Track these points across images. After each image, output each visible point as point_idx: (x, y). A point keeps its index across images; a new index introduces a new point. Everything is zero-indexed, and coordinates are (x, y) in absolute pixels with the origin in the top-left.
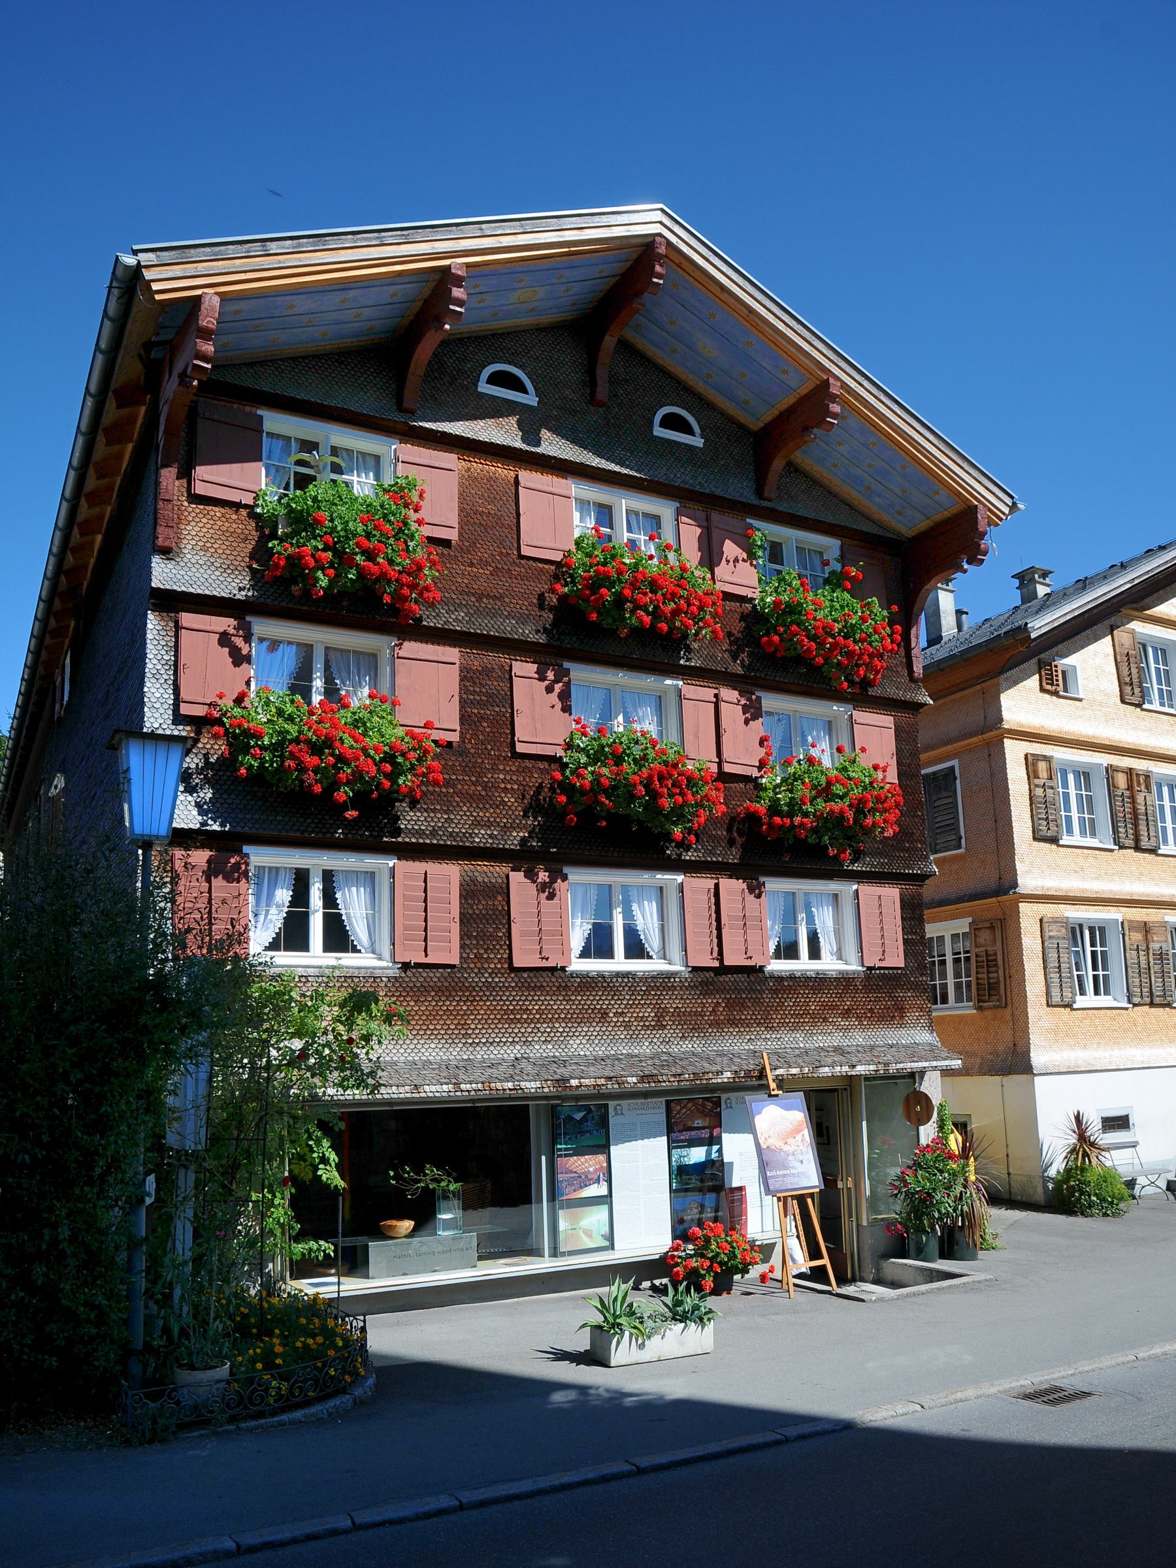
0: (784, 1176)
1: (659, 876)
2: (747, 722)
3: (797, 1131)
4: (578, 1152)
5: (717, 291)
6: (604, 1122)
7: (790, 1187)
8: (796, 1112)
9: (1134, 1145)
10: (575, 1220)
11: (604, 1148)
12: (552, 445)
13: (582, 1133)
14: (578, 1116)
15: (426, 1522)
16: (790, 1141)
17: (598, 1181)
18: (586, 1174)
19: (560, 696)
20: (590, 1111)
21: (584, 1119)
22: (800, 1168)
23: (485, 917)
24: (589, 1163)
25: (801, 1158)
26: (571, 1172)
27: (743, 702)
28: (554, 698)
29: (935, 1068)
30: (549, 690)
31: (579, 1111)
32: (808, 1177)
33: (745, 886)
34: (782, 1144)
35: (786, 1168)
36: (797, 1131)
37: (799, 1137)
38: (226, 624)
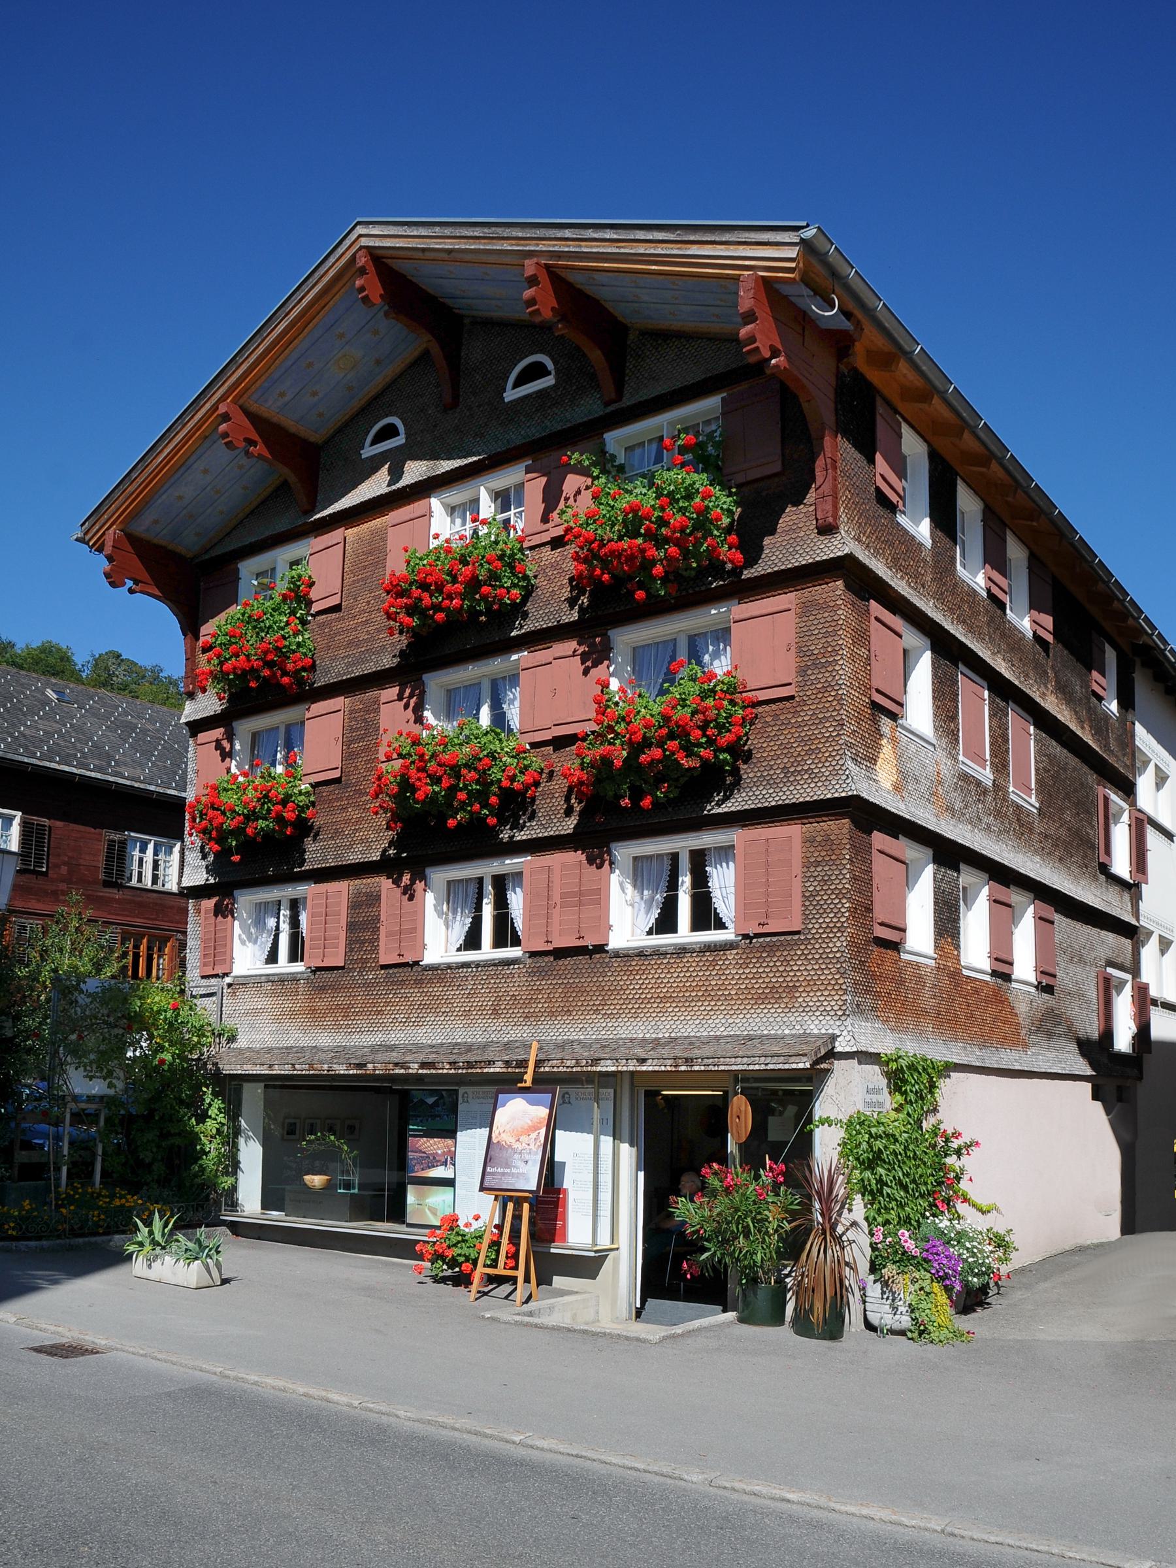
0: (503, 1174)
1: (508, 862)
2: (586, 672)
3: (535, 1128)
4: (429, 1134)
5: (420, 255)
6: (454, 1110)
7: (504, 1187)
8: (541, 1108)
9: (450, 1183)
10: (421, 1196)
11: (451, 1133)
12: (415, 471)
13: (434, 1117)
14: (430, 1101)
15: (584, 1454)
16: (524, 1138)
17: (445, 1163)
18: (435, 1155)
19: (414, 711)
20: (442, 1097)
21: (435, 1104)
22: (523, 1168)
23: (363, 926)
24: (435, 1146)
25: (527, 1157)
26: (421, 1151)
27: (582, 649)
28: (409, 713)
29: (865, 1057)
30: (406, 707)
31: (431, 1096)
32: (527, 1179)
33: (584, 857)
34: (513, 1141)
35: (508, 1166)
36: (535, 1128)
37: (533, 1135)
38: (218, 733)
